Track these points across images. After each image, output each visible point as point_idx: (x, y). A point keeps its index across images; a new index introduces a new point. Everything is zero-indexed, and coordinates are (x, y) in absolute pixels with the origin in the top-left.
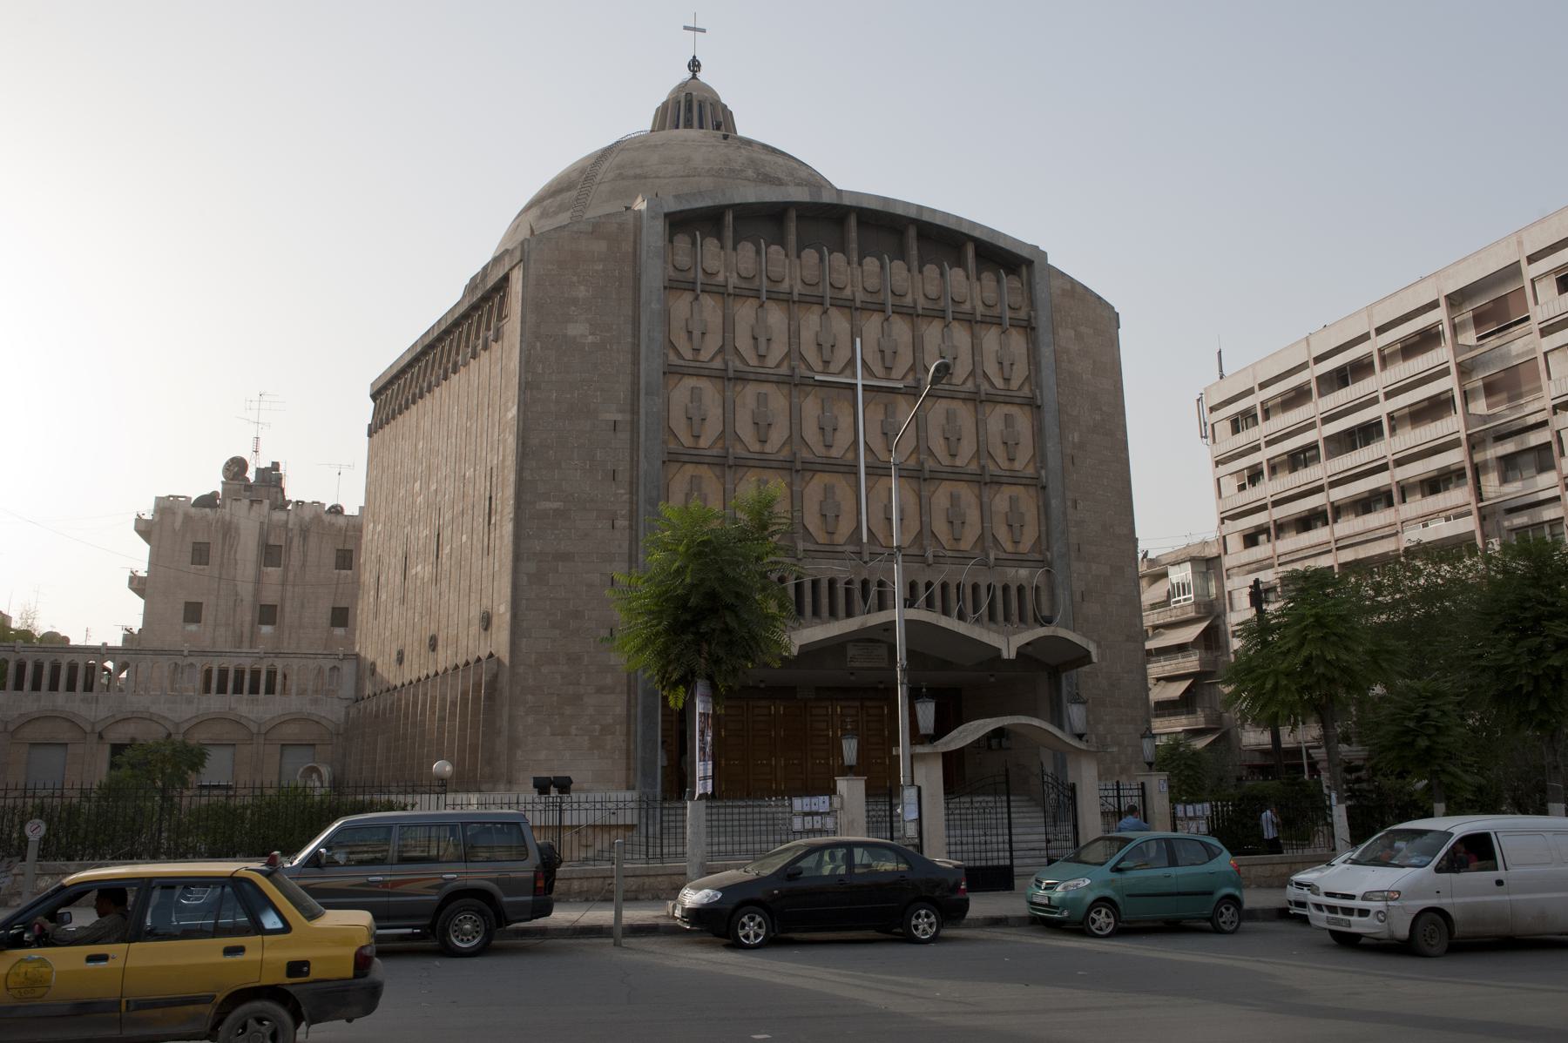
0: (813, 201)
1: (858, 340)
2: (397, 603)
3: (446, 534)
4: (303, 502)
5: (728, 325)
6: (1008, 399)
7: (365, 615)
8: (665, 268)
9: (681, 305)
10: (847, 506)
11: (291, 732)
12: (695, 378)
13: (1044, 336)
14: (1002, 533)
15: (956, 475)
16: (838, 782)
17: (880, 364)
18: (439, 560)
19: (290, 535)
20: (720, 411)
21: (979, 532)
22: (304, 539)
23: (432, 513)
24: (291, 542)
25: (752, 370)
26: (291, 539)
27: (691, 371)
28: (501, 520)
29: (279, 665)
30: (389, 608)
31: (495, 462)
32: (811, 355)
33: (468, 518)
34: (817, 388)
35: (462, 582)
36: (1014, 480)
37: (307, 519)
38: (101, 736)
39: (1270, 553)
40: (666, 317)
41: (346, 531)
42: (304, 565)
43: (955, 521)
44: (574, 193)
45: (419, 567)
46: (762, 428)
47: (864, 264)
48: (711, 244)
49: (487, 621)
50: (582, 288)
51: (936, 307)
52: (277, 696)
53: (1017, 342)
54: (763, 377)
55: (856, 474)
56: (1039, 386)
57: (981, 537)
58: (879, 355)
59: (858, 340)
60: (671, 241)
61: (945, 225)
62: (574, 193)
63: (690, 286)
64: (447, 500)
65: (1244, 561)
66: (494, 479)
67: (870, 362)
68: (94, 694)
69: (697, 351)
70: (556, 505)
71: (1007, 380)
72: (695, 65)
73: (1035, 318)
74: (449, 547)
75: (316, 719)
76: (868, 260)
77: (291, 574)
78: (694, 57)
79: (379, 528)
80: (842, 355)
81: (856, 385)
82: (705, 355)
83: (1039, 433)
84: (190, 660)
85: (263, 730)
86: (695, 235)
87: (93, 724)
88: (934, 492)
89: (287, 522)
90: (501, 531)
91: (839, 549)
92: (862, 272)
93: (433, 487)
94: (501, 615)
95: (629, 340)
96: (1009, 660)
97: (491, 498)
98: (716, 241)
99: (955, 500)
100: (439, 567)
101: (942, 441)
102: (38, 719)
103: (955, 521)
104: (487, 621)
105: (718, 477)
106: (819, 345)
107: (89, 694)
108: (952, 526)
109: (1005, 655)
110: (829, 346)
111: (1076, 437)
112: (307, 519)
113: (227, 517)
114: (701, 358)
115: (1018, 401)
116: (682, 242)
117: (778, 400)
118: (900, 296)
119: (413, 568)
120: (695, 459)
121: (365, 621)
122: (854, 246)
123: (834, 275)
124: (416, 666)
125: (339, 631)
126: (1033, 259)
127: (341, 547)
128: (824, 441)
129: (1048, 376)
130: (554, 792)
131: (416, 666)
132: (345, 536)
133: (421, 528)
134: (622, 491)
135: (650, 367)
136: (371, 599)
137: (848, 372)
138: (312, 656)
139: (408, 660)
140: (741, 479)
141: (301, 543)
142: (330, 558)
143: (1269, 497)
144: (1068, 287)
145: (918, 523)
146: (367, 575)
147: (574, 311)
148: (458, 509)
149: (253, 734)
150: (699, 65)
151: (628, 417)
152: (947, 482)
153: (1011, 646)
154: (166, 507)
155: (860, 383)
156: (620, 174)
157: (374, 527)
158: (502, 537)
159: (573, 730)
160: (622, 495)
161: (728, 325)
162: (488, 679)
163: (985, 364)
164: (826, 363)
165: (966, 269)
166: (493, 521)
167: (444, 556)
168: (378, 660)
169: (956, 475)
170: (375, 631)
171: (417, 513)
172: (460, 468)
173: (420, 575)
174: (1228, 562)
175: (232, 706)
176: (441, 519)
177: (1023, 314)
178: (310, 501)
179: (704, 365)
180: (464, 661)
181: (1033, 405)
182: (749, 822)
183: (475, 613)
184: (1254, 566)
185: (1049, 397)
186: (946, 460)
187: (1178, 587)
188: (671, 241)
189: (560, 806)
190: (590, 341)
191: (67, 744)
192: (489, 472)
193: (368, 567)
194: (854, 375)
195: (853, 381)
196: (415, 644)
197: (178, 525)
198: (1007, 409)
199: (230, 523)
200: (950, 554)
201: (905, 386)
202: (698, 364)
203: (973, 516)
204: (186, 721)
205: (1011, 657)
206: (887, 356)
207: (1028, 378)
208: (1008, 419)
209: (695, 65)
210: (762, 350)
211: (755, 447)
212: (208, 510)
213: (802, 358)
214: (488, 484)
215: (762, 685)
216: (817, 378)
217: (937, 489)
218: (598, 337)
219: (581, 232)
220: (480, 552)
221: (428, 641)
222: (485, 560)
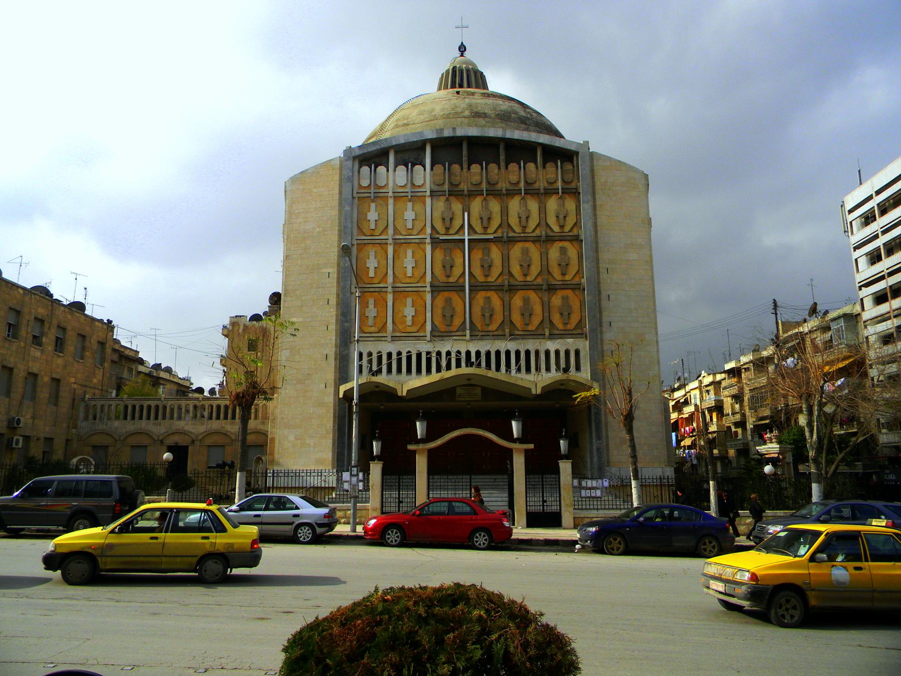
0: (439, 136)
1: (466, 214)
6: (562, 238)
10: (459, 309)
15: (527, 286)
16: (560, 464)
17: (480, 225)
34: (442, 244)
38: (162, 442)
39: (888, 309)
51: (515, 188)
52: (229, 420)
59: (466, 214)
61: (521, 138)
65: (874, 315)
68: (159, 421)
71: (562, 227)
72: (462, 49)
76: (473, 166)
78: (462, 43)
80: (457, 224)
81: (465, 239)
84: (203, 402)
85: (122, 438)
87: (120, 436)
99: (526, 301)
101: (518, 267)
102: (134, 433)
106: (443, 219)
107: (156, 421)
108: (484, 317)
109: (534, 392)
110: (449, 219)
113: (265, 325)
115: (569, 238)
117: (534, 252)
118: (493, 184)
122: (465, 159)
123: (453, 177)
128: (446, 273)
134: (332, 310)
137: (461, 233)
143: (885, 270)
145: (502, 316)
149: (233, 440)
152: (521, 291)
154: (235, 321)
156: (397, 124)
160: (332, 312)
163: (548, 219)
164: (447, 229)
165: (536, 163)
169: (527, 286)
174: (866, 316)
175: (223, 426)
181: (576, 239)
182: (464, 487)
184: (879, 318)
187: (409, 358)
191: (146, 446)
197: (241, 331)
198: (561, 244)
199: (266, 328)
203: (538, 309)
204: (201, 434)
206: (486, 221)
208: (563, 251)
209: (462, 49)
212: (255, 322)
215: (433, 411)
216: (440, 238)
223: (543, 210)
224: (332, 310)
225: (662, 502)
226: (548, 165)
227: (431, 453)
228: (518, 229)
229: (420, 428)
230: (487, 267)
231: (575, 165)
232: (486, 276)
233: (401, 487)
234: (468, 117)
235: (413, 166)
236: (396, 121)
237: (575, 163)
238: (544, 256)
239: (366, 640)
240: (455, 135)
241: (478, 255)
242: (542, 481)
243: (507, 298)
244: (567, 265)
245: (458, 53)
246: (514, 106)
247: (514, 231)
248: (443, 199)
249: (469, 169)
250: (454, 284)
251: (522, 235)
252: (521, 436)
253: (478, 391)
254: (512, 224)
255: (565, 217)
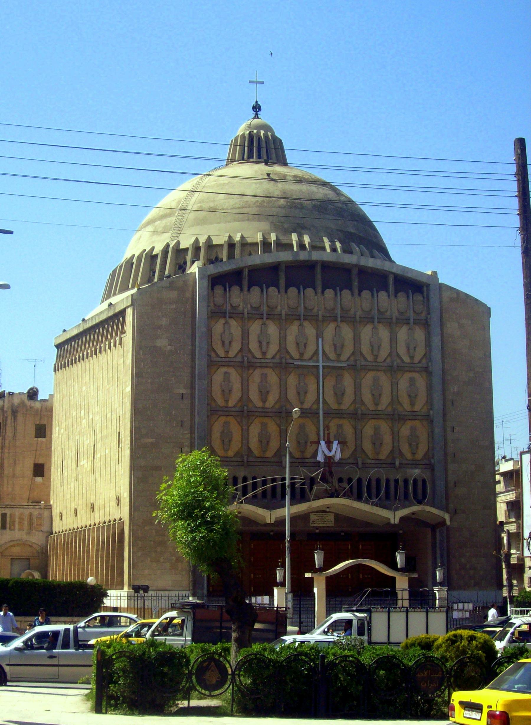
1: (320, 340)
2: (73, 480)
3: (98, 446)
4: (13, 393)
5: (245, 335)
7: (55, 483)
8: (208, 306)
9: (219, 327)
11: (16, 551)
12: (226, 367)
13: (436, 330)
14: (405, 449)
18: (95, 460)
19: (5, 415)
20: (240, 386)
21: (391, 449)
22: (15, 419)
23: (90, 432)
24: (6, 420)
25: (258, 361)
26: (6, 417)
27: (224, 364)
28: (124, 447)
29: (8, 511)
30: (69, 482)
31: (121, 413)
32: (295, 354)
33: (108, 441)
35: (106, 476)
36: (414, 416)
37: (16, 404)
40: (210, 333)
41: (41, 411)
42: (14, 436)
43: (377, 441)
44: (173, 219)
45: (85, 461)
46: (264, 395)
47: (325, 294)
48: (236, 289)
49: (118, 500)
50: (164, 319)
53: (419, 334)
54: (264, 365)
55: (318, 418)
56: (430, 360)
57: (392, 451)
58: (333, 347)
59: (320, 340)
60: (212, 289)
61: (374, 266)
62: (173, 219)
63: (223, 314)
64: (98, 427)
66: (121, 423)
67: (328, 352)
69: (227, 352)
70: (151, 440)
71: (412, 358)
72: (257, 108)
73: (430, 318)
74: (100, 454)
75: (29, 543)
77: (7, 442)
78: (257, 102)
79: (62, 431)
81: (319, 366)
82: (232, 354)
83: (430, 388)
86: (226, 284)
88: (365, 426)
89: (3, 407)
90: (124, 453)
91: (307, 461)
92: (324, 298)
93: (91, 417)
94: (125, 498)
95: (190, 348)
96: (395, 524)
97: (119, 433)
98: (238, 287)
99: (377, 430)
100: (95, 464)
101: (370, 396)
103: (377, 441)
104: (118, 500)
105: (238, 422)
111: (455, 389)
112: (16, 404)
114: (230, 356)
115: (418, 369)
116: (219, 290)
119: (81, 461)
120: (227, 413)
121: (55, 486)
124: (84, 518)
125: (39, 479)
126: (429, 283)
127: (38, 423)
129: (436, 355)
130: (141, 592)
131: (84, 518)
132: (41, 415)
133: (85, 439)
134: (186, 432)
135: (200, 364)
136: (59, 474)
138: (26, 507)
139: (80, 514)
140: (251, 423)
141: (13, 420)
142: (32, 431)
144: (455, 296)
146: (56, 458)
147: (160, 333)
148: (104, 433)
150: (260, 108)
151: (189, 391)
153: (396, 517)
155: (321, 364)
156: (201, 207)
157: (59, 430)
158: (124, 456)
159: (162, 560)
161: (245, 335)
162: (119, 532)
164: (302, 354)
166: (120, 446)
167: (97, 459)
168: (64, 511)
169: (377, 415)
170: (62, 494)
171: (83, 429)
172: (104, 411)
173: (85, 466)
176: (95, 437)
177: (423, 316)
178: (17, 392)
179: (232, 360)
180: (108, 520)
181: (427, 371)
183: (113, 495)
185: (436, 367)
186: (372, 407)
188: (212, 289)
189: (144, 598)
190: (168, 349)
192: (118, 418)
193: (56, 453)
194: (318, 361)
195: (317, 364)
196: (84, 505)
198: (410, 375)
200: (373, 462)
201: (348, 365)
202: (227, 359)
205: (396, 523)
206: (338, 348)
207: (425, 355)
208: (412, 381)
210: (264, 349)
211: (260, 405)
213: (288, 352)
214: (118, 424)
216: (295, 363)
217: (366, 424)
218: (173, 347)
219: (163, 287)
220: (115, 461)
221: (90, 505)
222: (117, 466)
223: (393, 339)
224: (186, 432)
225: (91, 666)
226: (400, 294)
227: (330, 580)
228: (370, 358)
229: (318, 558)
230: (339, 395)
231: (425, 296)
232: (340, 404)
233: (302, 612)
234: (284, 207)
235: (267, 288)
236: (200, 202)
237: (425, 293)
238: (394, 385)
239: (479, 685)
240: (310, 259)
241: (330, 383)
242: (300, 607)
243: (245, 375)
244: (416, 395)
245: (253, 114)
246: (329, 194)
247: (366, 360)
248: (296, 323)
249: (323, 293)
250: (308, 411)
251: (374, 364)
252: (404, 566)
253: (331, 517)
254: (364, 352)
255: (415, 348)
